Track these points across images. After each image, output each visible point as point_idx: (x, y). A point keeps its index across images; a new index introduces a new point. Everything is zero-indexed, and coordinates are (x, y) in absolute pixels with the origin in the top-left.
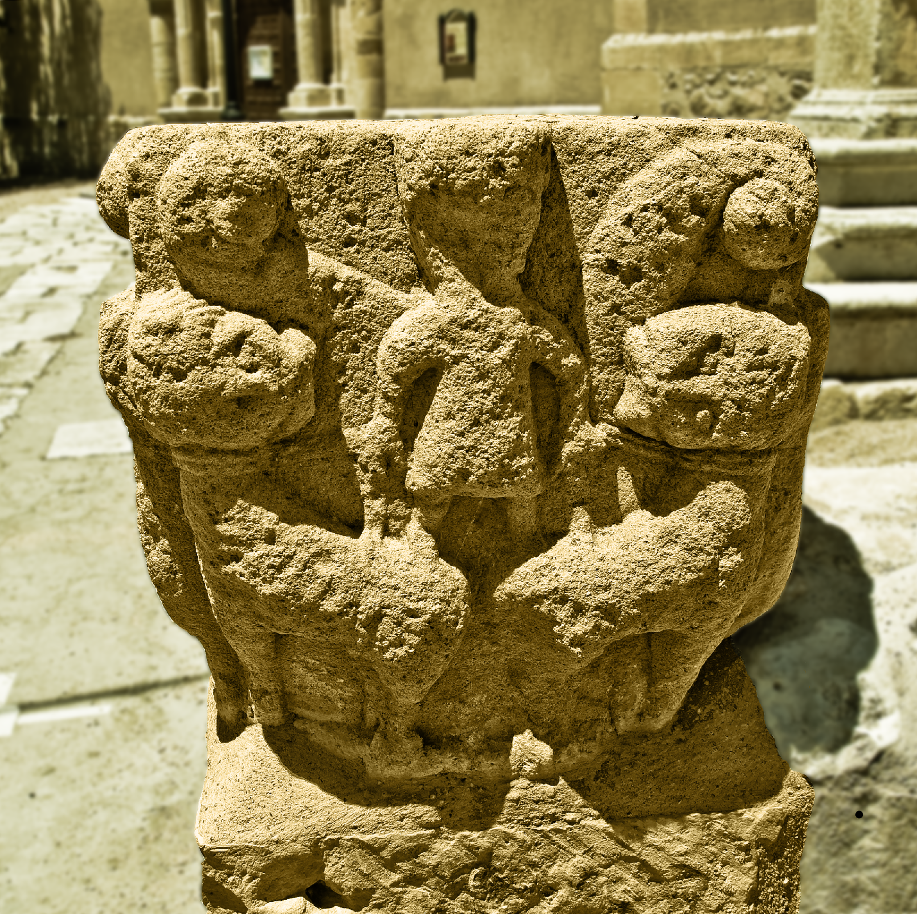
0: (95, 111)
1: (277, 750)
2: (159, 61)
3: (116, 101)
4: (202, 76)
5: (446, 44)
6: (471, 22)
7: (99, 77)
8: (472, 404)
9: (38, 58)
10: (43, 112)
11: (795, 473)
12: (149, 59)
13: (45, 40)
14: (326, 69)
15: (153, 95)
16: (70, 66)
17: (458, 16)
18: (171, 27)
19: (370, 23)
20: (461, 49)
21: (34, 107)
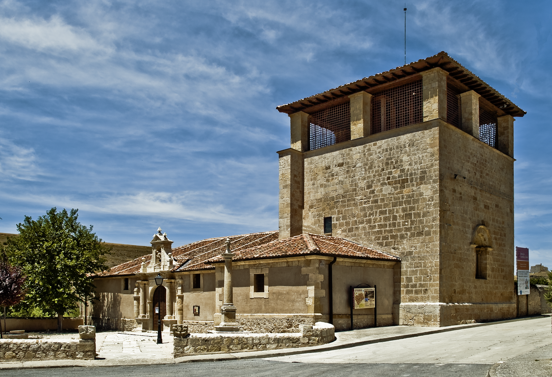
0: (118, 317)
1: (480, 119)
2: (135, 309)
3: (123, 316)
4: (145, 312)
5: (194, 310)
6: (199, 307)
7: (119, 310)
8: (83, 271)
9: (103, 306)
10: (103, 317)
11: (455, 317)
12: (133, 308)
13: (106, 302)
14: (172, 313)
15: (133, 315)
16: (111, 308)
17: (197, 306)
18: (139, 303)
19: (181, 306)
20: (197, 312)
21: (101, 315)
